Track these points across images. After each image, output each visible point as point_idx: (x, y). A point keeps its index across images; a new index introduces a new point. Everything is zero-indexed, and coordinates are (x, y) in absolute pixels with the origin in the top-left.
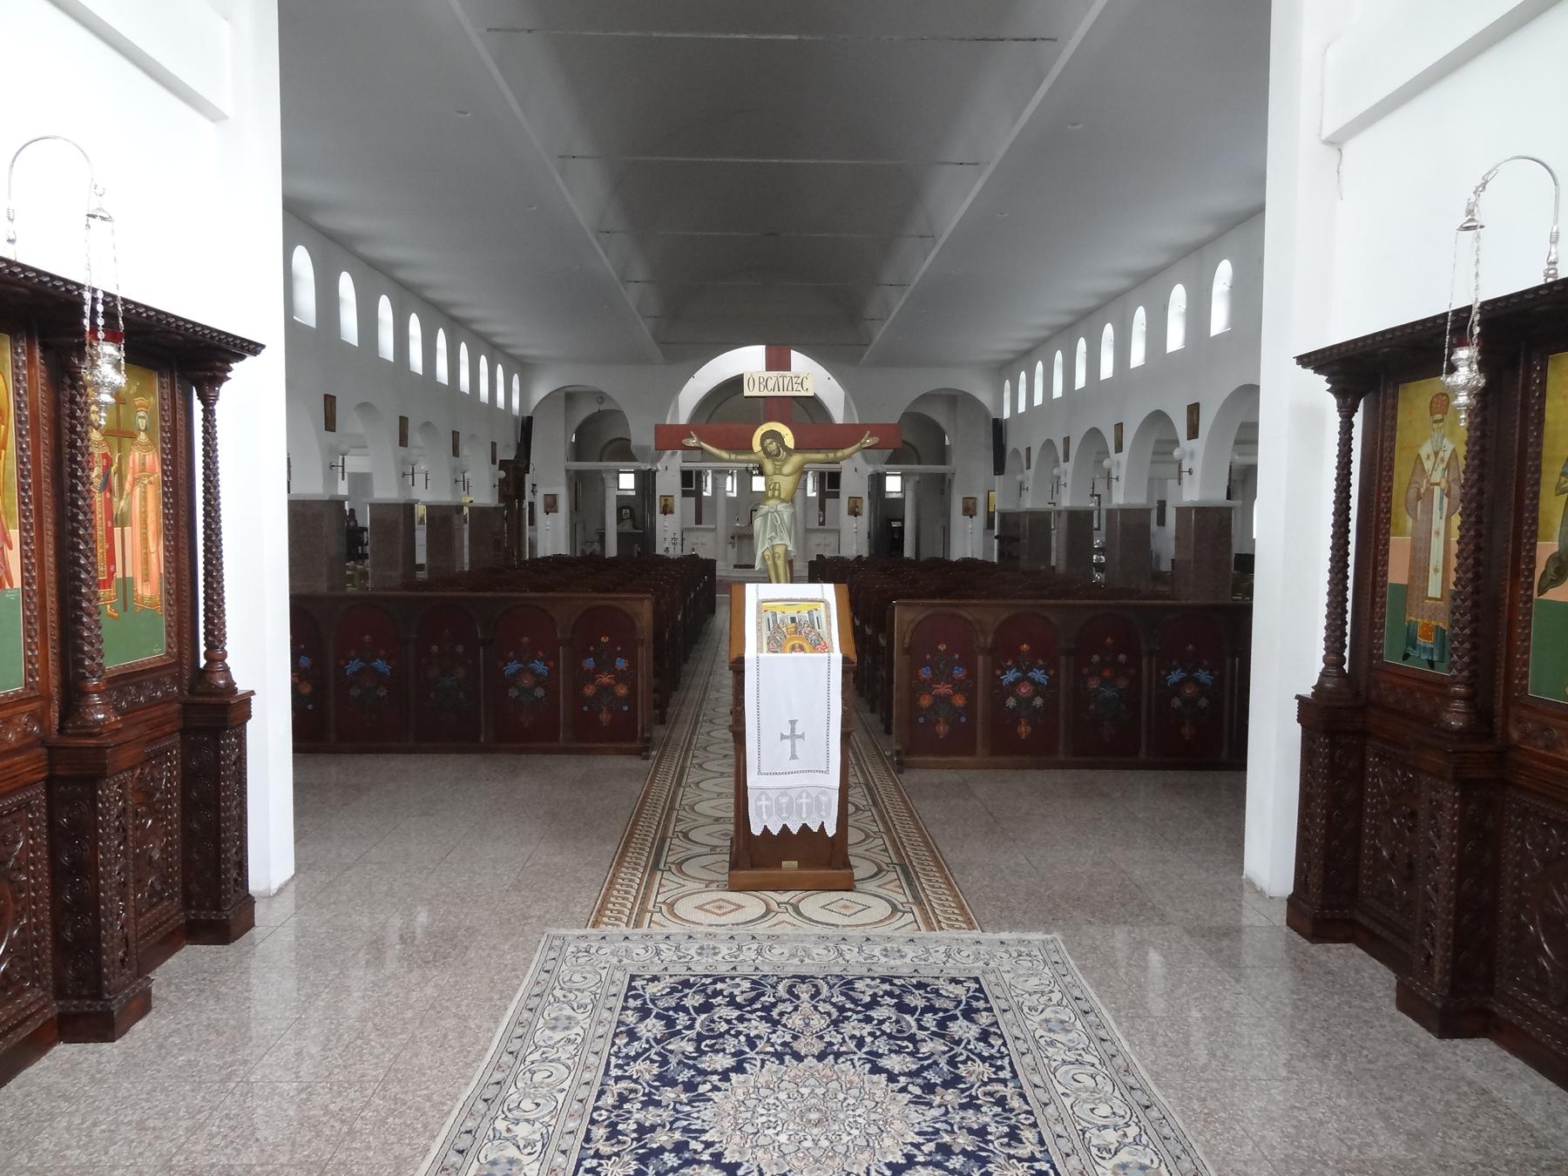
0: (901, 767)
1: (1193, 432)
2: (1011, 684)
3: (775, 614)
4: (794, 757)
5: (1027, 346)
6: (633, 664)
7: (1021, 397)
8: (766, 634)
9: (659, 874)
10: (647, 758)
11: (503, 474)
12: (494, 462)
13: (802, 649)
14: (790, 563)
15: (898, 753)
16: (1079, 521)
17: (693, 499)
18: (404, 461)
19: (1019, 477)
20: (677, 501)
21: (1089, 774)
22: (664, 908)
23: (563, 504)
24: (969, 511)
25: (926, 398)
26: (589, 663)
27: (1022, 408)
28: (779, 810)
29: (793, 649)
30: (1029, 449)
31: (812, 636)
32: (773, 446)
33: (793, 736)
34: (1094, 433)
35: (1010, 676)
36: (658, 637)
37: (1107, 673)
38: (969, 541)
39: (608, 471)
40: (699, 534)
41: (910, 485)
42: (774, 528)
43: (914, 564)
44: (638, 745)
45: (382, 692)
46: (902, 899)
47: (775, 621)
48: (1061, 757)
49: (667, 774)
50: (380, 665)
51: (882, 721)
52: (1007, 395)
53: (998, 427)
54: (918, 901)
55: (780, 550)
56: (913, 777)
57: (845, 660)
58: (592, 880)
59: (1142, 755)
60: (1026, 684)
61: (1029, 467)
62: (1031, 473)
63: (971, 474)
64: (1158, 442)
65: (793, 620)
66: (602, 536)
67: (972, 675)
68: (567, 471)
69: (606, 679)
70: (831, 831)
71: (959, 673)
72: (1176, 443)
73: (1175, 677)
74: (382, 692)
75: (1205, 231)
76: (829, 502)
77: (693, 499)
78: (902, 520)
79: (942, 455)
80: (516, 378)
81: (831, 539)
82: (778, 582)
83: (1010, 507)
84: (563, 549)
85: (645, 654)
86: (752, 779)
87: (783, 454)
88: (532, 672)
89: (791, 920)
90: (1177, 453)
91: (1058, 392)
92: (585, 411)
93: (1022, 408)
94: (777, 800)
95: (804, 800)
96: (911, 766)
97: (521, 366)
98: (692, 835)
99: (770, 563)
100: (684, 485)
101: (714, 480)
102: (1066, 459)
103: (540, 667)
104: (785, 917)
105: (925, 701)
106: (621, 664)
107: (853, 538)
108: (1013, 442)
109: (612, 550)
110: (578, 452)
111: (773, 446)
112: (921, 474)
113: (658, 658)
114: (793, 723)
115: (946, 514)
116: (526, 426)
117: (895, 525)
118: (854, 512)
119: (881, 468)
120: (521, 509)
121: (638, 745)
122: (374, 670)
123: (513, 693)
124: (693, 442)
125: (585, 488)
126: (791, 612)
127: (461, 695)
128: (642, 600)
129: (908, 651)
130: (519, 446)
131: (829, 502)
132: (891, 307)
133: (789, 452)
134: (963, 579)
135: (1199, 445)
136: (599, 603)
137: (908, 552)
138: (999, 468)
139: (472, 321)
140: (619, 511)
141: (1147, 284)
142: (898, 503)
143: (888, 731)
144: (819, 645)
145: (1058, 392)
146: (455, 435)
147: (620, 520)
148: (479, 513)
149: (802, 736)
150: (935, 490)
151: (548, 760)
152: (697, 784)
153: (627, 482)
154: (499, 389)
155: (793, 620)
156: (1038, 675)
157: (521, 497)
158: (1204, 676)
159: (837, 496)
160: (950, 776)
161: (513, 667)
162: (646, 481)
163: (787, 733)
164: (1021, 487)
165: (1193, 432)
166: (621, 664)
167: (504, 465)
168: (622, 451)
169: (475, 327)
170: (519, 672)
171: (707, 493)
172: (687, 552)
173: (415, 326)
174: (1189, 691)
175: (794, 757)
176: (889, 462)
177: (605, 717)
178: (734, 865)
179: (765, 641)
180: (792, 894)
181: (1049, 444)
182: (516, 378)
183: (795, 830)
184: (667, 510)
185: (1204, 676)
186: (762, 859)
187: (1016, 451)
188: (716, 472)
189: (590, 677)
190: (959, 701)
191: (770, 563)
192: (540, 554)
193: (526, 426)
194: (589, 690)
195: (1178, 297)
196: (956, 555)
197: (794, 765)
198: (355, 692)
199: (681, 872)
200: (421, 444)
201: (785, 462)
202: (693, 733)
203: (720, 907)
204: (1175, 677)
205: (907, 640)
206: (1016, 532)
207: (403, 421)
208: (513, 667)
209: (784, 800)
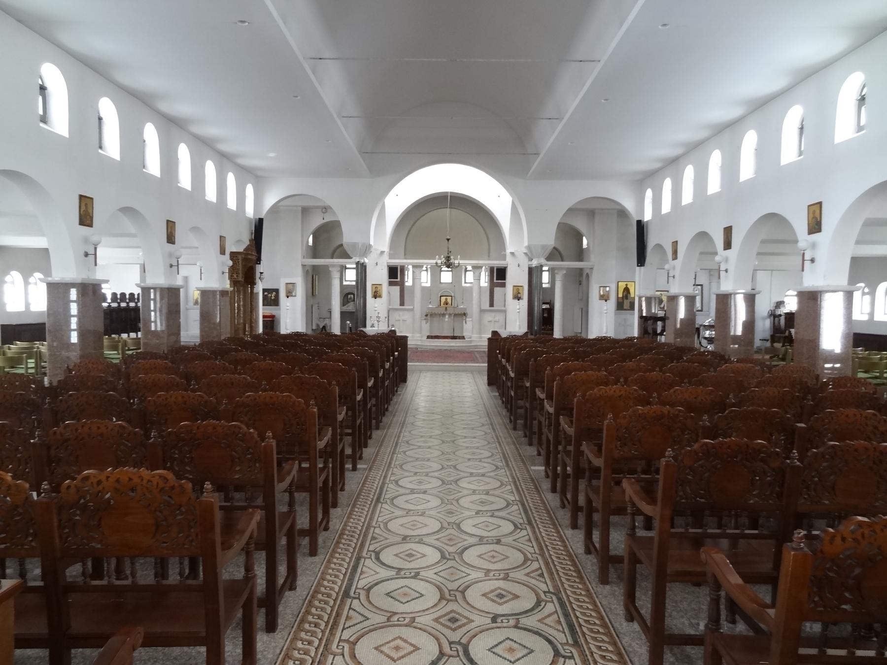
1: (728, 245)
12: (223, 252)
17: (398, 288)
18: (170, 255)
20: (385, 289)
22: (373, 555)
24: (605, 298)
25: (571, 211)
30: (675, 244)
39: (334, 266)
40: (401, 313)
46: (544, 587)
51: (511, 421)
53: (641, 227)
63: (609, 270)
68: (304, 266)
72: (716, 253)
75: (780, 83)
76: (497, 290)
77: (398, 288)
79: (580, 254)
81: (499, 317)
89: (456, 534)
92: (317, 221)
97: (250, 175)
100: (390, 277)
104: (451, 549)
108: (651, 243)
110: (315, 252)
116: (258, 226)
118: (517, 297)
125: (316, 278)
131: (497, 290)
132: (549, 137)
135: (732, 253)
138: (641, 260)
152: (405, 453)
153: (351, 276)
165: (728, 245)
167: (233, 255)
168: (342, 252)
169: (240, 161)
171: (409, 282)
184: (376, 295)
187: (659, 247)
188: (414, 267)
195: (668, 184)
196: (594, 333)
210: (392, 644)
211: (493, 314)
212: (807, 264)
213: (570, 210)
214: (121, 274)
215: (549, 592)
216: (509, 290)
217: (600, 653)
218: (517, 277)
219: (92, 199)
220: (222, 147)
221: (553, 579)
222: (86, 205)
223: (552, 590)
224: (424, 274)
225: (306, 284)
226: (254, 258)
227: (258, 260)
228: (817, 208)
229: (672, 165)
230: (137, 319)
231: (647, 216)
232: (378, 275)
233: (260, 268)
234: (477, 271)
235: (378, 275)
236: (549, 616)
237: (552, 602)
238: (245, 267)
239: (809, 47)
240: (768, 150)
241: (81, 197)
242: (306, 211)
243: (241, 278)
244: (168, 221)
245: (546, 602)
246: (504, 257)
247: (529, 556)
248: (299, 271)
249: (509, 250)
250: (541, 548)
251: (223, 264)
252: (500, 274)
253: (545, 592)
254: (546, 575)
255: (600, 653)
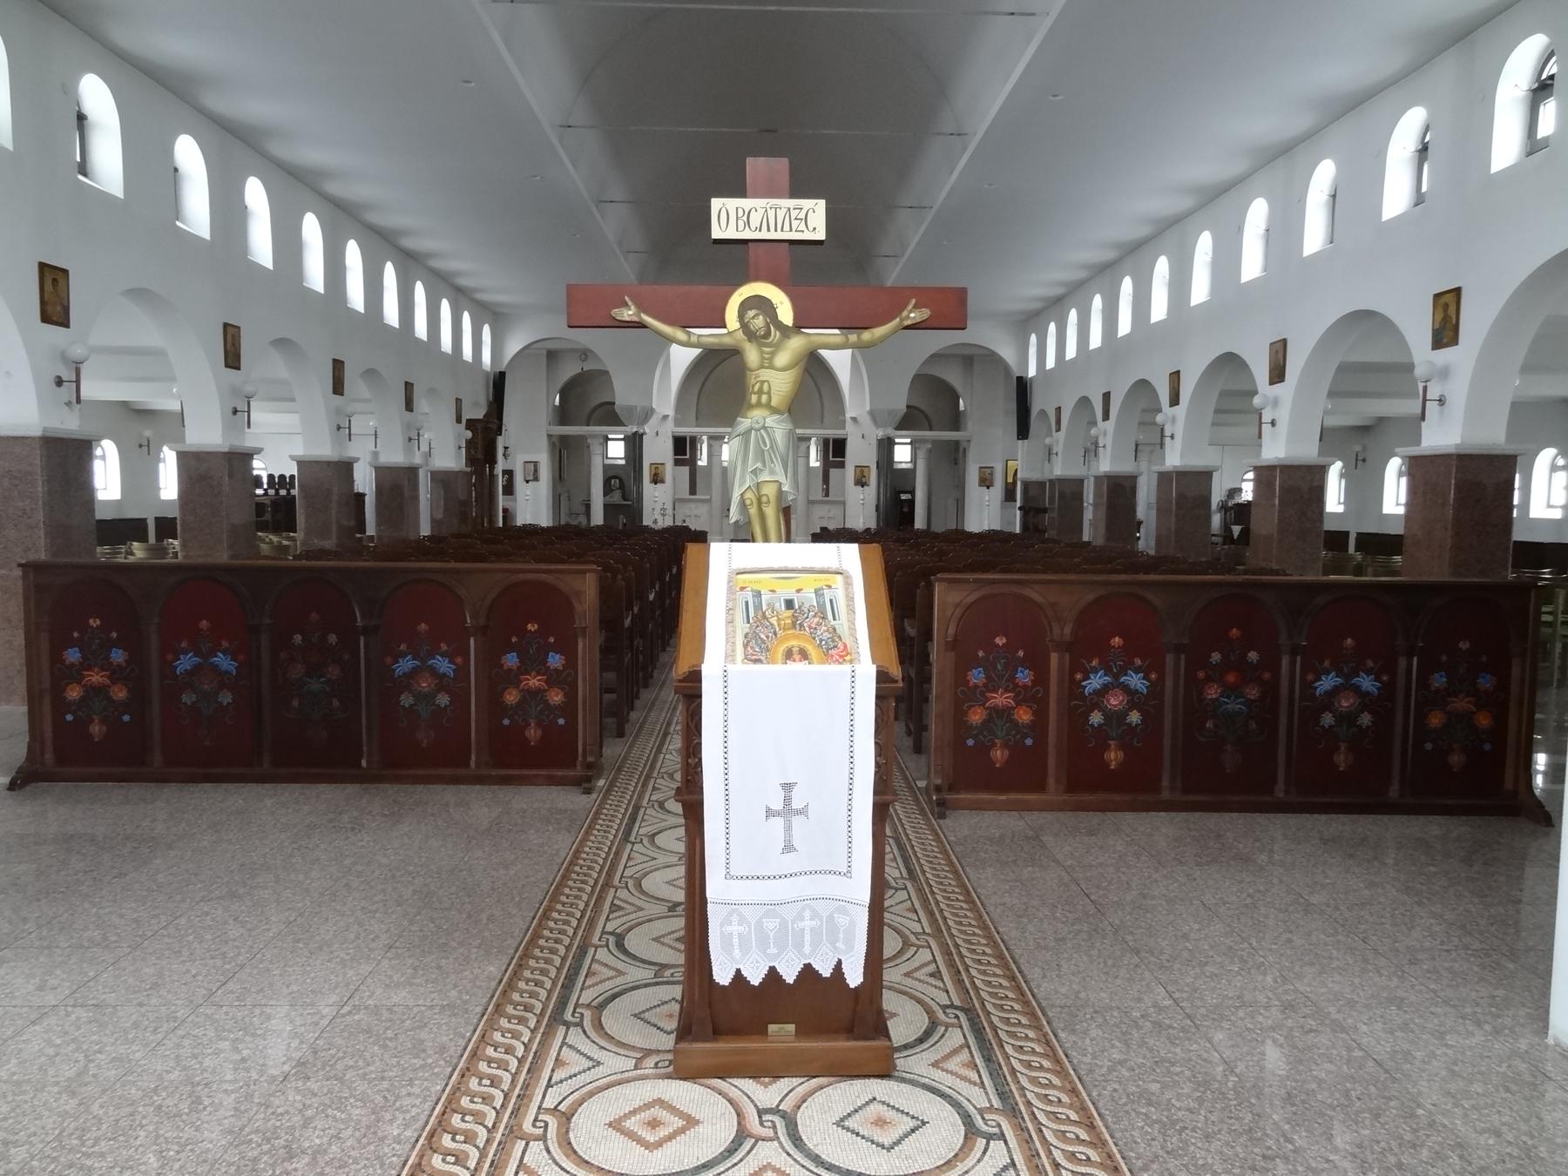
0: (942, 808)
2: (1096, 692)
3: (758, 594)
4: (789, 848)
5: (1059, 291)
6: (571, 662)
7: (1041, 356)
8: (741, 628)
9: (562, 1030)
10: (588, 791)
11: (469, 434)
12: (459, 420)
13: (804, 655)
14: (786, 512)
15: (938, 789)
16: (1119, 491)
17: (686, 469)
19: (1048, 441)
20: (669, 470)
21: (1213, 820)
23: (545, 473)
24: (986, 482)
25: (936, 357)
26: (511, 660)
27: (1050, 363)
28: (763, 942)
29: (789, 655)
30: (1059, 410)
31: (822, 632)
32: (759, 322)
33: (788, 811)
34: (1143, 386)
35: (1095, 682)
36: (609, 623)
37: (1231, 678)
38: (985, 513)
39: (594, 436)
40: (693, 505)
41: (921, 454)
42: (760, 455)
43: (927, 533)
44: (579, 771)
45: (226, 698)
47: (758, 607)
48: (1166, 795)
49: (612, 819)
50: (223, 661)
51: (909, 733)
52: (1033, 351)
53: (1023, 387)
54: (1012, 1112)
55: (769, 491)
56: (963, 825)
57: (882, 677)
58: (442, 1049)
59: (1280, 793)
60: (1115, 691)
61: (1058, 430)
62: (1061, 435)
63: (991, 444)
64: (1224, 394)
65: (789, 604)
66: (588, 507)
67: (1041, 678)
68: (550, 436)
69: (534, 682)
70: (854, 977)
71: (1024, 677)
72: (1160, 410)
73: (1327, 683)
74: (226, 698)
75: (1300, 123)
76: (833, 472)
78: (912, 492)
80: (486, 330)
81: (836, 511)
82: (766, 539)
83: (1035, 476)
84: (544, 520)
85: (587, 649)
86: (716, 887)
87: (775, 335)
88: (433, 671)
90: (1257, 401)
91: (1095, 341)
92: (569, 370)
93: (1050, 363)
94: (759, 924)
95: (807, 924)
96: (958, 806)
97: (492, 315)
98: (631, 942)
99: (753, 511)
101: (710, 446)
102: (1106, 416)
103: (443, 665)
105: (976, 717)
106: (555, 660)
107: (861, 507)
109: (598, 518)
110: (563, 415)
111: (759, 322)
112: (935, 442)
113: (609, 651)
114: (788, 787)
115: (960, 487)
116: (499, 382)
117: (903, 497)
118: (861, 482)
119: (890, 432)
120: (492, 476)
121: (579, 771)
122: (215, 667)
123: (406, 700)
124: (628, 314)
126: (786, 590)
127: (336, 703)
128: (584, 572)
129: (953, 645)
130: (490, 405)
131: (833, 472)
133: (785, 331)
134: (988, 551)
135: (1181, 411)
136: (522, 577)
137: (919, 523)
138: (1023, 431)
139: (429, 255)
140: (607, 482)
141: (1217, 201)
142: (909, 474)
143: (918, 749)
144: (834, 650)
145: (1095, 341)
146: (409, 386)
147: (607, 489)
148: (442, 479)
149: (803, 812)
150: (950, 458)
151: (447, 794)
152: (652, 837)
153: (616, 450)
154: (478, 347)
155: (789, 604)
156: (1135, 681)
157: (492, 461)
158: (1367, 683)
159: (842, 465)
160: (1012, 823)
161: (406, 665)
162: (634, 444)
163: (778, 805)
164: (1050, 452)
166: (555, 660)
167: (471, 424)
168: (609, 415)
170: (415, 672)
171: (703, 462)
172: (679, 523)
173: (353, 254)
174: (1345, 703)
175: (789, 848)
176: (898, 428)
177: (533, 733)
178: (685, 1032)
179: (740, 640)
180: (784, 1084)
181: (1085, 402)
182: (486, 330)
183: (789, 975)
184: (657, 479)
185: (1367, 683)
186: (728, 1024)
187: (1043, 413)
188: (711, 438)
189: (512, 678)
190: (1024, 716)
191: (753, 511)
192: (519, 522)
193: (499, 382)
194: (511, 697)
197: (790, 863)
198: (188, 698)
199: (599, 1026)
200: (367, 394)
201: (777, 347)
202: (659, 751)
203: (654, 1124)
204: (1327, 683)
205: (951, 631)
206: (1045, 505)
207: (338, 365)
208: (406, 665)
209: (771, 925)
210: (663, 1132)
211: (826, 507)
212: (1266, 428)
213: (934, 356)
214: (280, 448)
215: (952, 1006)
216: (850, 472)
217: (1055, 1126)
218: (860, 452)
219: (65, 272)
220: (408, 243)
221: (959, 982)
222: (55, 280)
223: (957, 1003)
224: (725, 448)
225: (553, 462)
226: (494, 427)
227: (499, 431)
228: (1449, 298)
229: (1054, 307)
230: (1401, 545)
231: (1032, 372)
232: (658, 450)
233: (501, 442)
234: (803, 446)
235: (658, 450)
236: (955, 1052)
237: (1002, 1137)
238: (484, 438)
239: (1340, 70)
240: (1285, 229)
241: (43, 267)
242: (552, 356)
243: (480, 456)
244: (226, 325)
245: (947, 1026)
246: (843, 425)
247: (913, 939)
248: (544, 443)
249: (848, 416)
250: (910, 871)
251: (459, 436)
252: (835, 450)
253: (981, 1111)
254: (946, 977)
255: (1055, 1126)
